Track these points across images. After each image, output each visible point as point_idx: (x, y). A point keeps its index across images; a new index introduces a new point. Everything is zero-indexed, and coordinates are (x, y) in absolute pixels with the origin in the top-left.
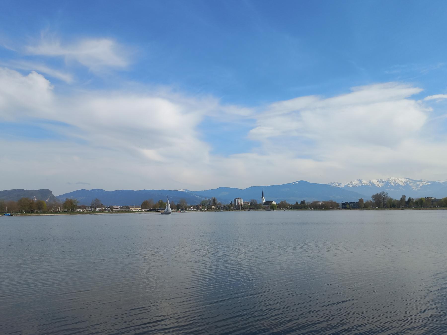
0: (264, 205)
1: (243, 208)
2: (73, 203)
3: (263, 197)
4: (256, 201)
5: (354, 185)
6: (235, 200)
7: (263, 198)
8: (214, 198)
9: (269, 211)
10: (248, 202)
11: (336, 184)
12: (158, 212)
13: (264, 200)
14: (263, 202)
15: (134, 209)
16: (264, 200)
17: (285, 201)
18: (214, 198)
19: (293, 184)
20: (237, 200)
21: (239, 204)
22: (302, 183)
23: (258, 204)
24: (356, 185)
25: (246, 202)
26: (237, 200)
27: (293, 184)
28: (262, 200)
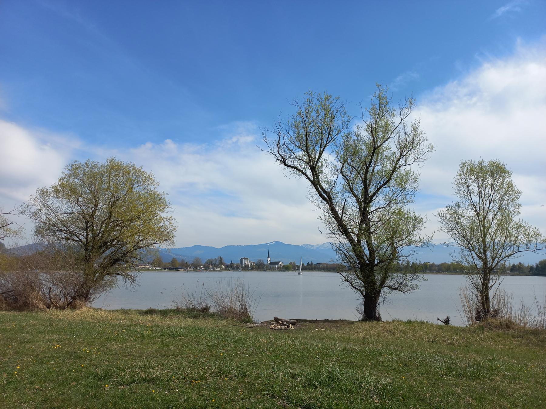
0: (270, 266)
1: (246, 268)
2: (10, 249)
3: (268, 257)
4: (263, 261)
5: (325, 247)
6: (241, 260)
7: (269, 259)
8: (221, 257)
9: (452, 275)
10: (253, 262)
11: (309, 246)
12: (178, 270)
13: (269, 260)
14: (269, 262)
15: (12, 265)
16: (269, 260)
17: (294, 262)
18: (221, 257)
19: (269, 244)
20: (244, 259)
21: (245, 264)
22: (278, 244)
23: (518, 264)
24: (327, 247)
25: (252, 262)
26: (244, 259)
27: (269, 244)
28: (268, 260)
